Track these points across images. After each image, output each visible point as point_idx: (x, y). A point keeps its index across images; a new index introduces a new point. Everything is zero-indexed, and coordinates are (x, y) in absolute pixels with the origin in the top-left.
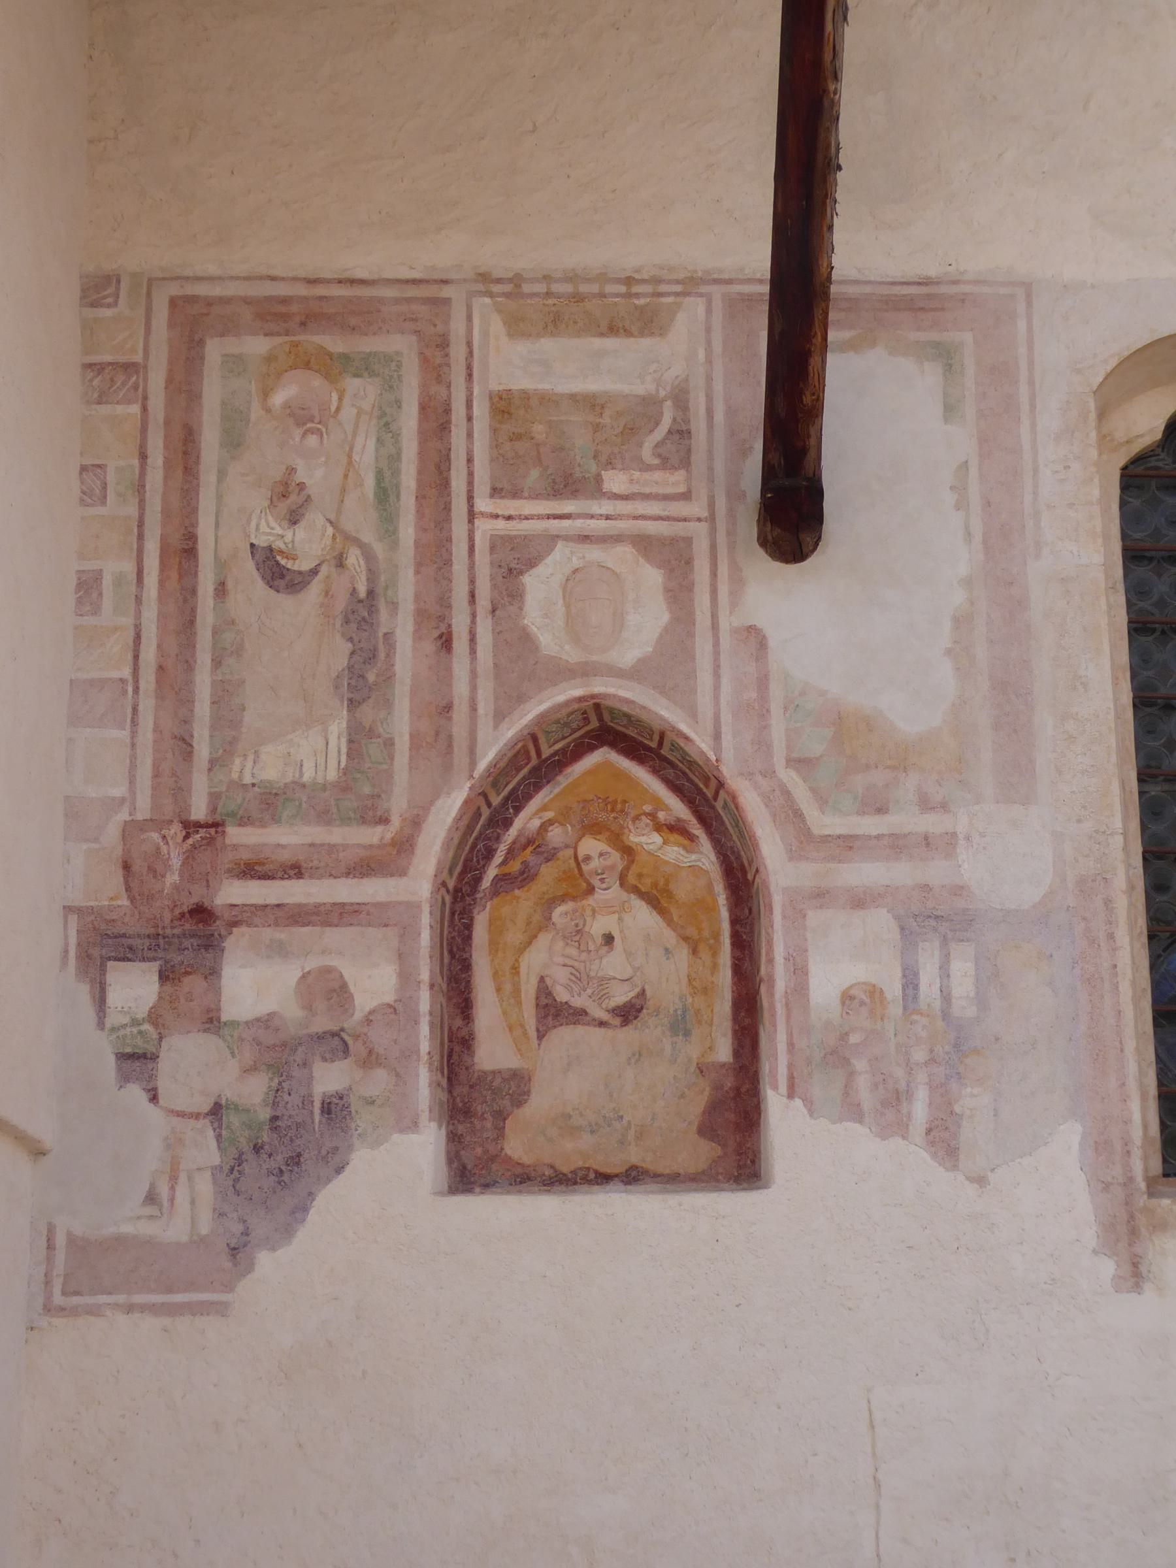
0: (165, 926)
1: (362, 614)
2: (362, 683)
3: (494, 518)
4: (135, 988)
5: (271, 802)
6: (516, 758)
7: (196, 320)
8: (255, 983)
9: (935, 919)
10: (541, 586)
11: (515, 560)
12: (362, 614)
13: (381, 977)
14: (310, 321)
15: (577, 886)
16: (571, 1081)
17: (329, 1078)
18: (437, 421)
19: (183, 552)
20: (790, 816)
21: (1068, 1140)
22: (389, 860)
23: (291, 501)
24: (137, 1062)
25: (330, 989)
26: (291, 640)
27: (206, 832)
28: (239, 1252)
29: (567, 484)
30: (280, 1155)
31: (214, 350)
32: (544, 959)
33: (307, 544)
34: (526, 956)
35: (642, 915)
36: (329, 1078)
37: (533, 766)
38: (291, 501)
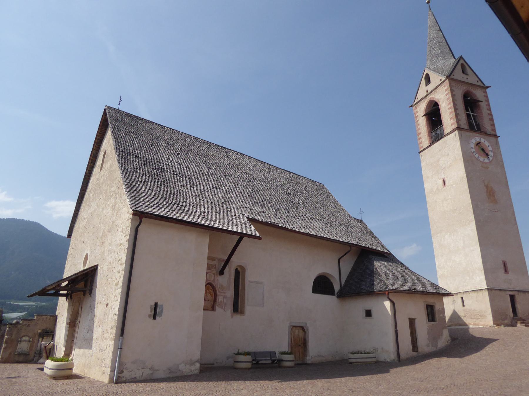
9: (225, 297)
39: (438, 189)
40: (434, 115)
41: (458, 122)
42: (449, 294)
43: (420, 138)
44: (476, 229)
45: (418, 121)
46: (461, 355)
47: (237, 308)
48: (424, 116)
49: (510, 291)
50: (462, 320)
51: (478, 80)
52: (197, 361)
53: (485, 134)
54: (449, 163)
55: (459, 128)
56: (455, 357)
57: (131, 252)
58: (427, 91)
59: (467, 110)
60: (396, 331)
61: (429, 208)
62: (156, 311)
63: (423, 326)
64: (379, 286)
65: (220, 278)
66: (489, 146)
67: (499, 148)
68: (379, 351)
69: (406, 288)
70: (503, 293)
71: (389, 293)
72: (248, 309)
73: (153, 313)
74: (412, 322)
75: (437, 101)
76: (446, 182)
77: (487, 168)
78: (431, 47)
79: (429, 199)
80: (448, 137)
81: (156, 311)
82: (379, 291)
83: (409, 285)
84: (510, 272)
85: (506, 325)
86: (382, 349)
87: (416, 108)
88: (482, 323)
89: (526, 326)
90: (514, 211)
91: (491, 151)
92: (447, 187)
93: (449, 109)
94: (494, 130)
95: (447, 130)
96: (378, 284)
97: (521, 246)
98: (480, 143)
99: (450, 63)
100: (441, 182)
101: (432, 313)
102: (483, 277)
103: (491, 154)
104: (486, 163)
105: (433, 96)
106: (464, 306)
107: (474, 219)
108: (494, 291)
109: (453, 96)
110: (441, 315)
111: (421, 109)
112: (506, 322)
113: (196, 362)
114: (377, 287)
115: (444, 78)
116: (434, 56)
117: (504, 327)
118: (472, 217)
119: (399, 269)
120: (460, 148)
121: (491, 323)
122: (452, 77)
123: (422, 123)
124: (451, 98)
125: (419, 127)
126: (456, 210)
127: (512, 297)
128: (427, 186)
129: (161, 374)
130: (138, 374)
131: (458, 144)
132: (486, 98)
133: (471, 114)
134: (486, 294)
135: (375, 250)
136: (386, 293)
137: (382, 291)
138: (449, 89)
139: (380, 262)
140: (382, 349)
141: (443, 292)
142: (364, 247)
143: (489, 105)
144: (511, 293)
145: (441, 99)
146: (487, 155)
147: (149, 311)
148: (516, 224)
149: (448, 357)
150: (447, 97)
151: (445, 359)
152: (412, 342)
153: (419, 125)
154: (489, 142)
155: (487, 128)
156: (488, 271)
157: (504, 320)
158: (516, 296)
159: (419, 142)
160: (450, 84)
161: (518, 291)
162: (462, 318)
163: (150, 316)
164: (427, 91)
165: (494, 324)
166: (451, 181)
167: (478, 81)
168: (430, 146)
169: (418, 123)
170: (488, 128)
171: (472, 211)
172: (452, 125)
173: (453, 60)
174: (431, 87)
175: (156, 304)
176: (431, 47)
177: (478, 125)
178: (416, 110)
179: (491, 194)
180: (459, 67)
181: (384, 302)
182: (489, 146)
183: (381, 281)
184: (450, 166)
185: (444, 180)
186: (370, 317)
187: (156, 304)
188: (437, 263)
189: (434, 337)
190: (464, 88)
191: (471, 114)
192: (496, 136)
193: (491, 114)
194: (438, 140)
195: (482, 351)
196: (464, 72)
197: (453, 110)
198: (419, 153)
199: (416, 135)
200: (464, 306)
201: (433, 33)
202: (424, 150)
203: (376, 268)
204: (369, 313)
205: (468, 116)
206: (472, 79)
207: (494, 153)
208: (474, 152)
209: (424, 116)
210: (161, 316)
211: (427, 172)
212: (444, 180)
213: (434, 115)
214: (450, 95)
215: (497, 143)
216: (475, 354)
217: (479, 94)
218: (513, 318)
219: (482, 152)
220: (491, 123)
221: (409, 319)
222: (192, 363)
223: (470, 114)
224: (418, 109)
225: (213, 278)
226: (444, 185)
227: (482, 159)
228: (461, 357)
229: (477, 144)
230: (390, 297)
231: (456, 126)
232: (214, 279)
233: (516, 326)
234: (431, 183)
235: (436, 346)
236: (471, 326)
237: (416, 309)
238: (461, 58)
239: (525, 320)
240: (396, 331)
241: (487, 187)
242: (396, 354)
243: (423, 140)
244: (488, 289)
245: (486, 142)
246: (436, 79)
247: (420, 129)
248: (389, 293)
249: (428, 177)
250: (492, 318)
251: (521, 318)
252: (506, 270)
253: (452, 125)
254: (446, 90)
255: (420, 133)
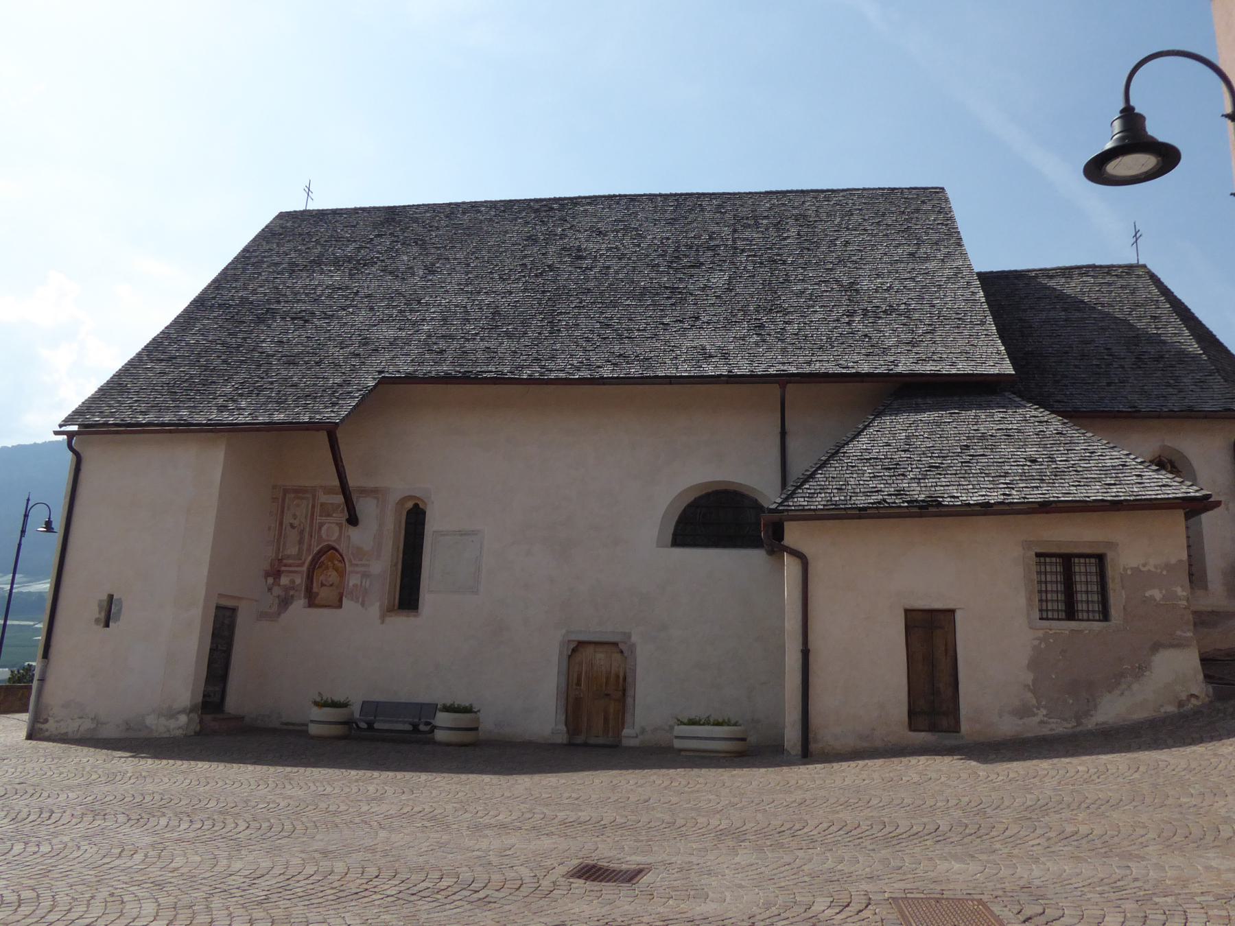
0: (275, 573)
1: (302, 532)
2: (301, 542)
3: (318, 520)
4: (270, 580)
5: (289, 557)
6: (319, 552)
7: (286, 491)
8: (284, 580)
9: (365, 575)
10: (324, 529)
11: (321, 525)
12: (302, 532)
13: (299, 580)
14: (299, 491)
15: (327, 568)
16: (324, 594)
17: (292, 593)
18: (313, 507)
19: (281, 524)
20: (350, 561)
21: (378, 604)
22: (301, 565)
23: (295, 517)
24: (270, 590)
25: (293, 582)
26: (293, 535)
27: (280, 561)
28: (279, 614)
29: (329, 515)
30: (285, 602)
31: (288, 496)
32: (322, 578)
33: (296, 523)
34: (319, 577)
35: (334, 573)
36: (292, 593)
37: (322, 552)
38: (295, 517)
47: (407, 597)
52: (183, 711)
57: (68, 500)
62: (109, 613)
65: (354, 533)
72: (428, 598)
73: (103, 614)
81: (109, 613)
113: (179, 712)
129: (108, 732)
130: (71, 727)
147: (94, 612)
163: (97, 621)
175: (111, 597)
187: (111, 597)
210: (117, 619)
221: (907, 611)
222: (172, 715)
225: (336, 534)
232: (340, 536)
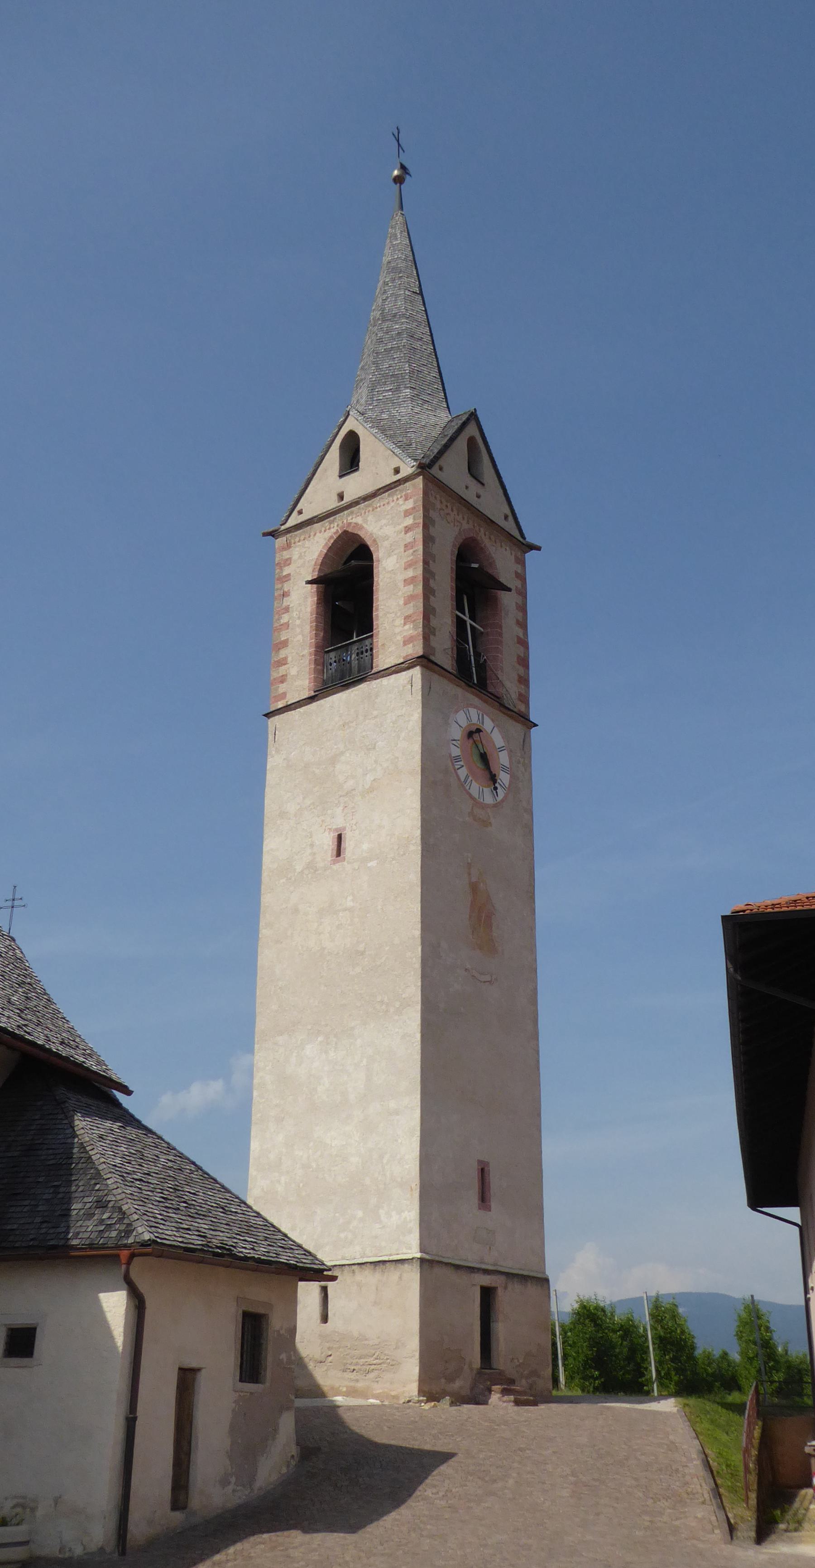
39: (311, 866)
40: (347, 589)
41: (426, 638)
42: (318, 1273)
43: (283, 662)
44: (418, 1036)
45: (285, 595)
46: (351, 1521)
48: (309, 582)
49: (486, 1272)
50: (310, 1376)
51: (508, 511)
53: (498, 702)
54: (369, 778)
55: (425, 661)
56: (331, 1527)
58: (341, 497)
59: (460, 607)
60: (131, 1423)
61: (265, 932)
63: (220, 1397)
64: (90, 1225)
66: (501, 749)
67: (528, 766)
68: (39, 1513)
69: (197, 1242)
70: (462, 1279)
71: (133, 1256)
74: (187, 1378)
75: (369, 543)
76: (348, 844)
77: (486, 823)
78: (380, 341)
79: (272, 897)
80: (385, 681)
82: (91, 1246)
83: (203, 1225)
84: (493, 1205)
85: (459, 1400)
86: (57, 1501)
87: (288, 546)
88: (378, 1389)
89: (517, 1403)
90: (535, 990)
91: (504, 769)
92: (346, 866)
93: (407, 582)
94: (524, 698)
95: (384, 658)
96: (89, 1216)
97: (539, 1115)
98: (479, 731)
99: (433, 420)
100: (328, 842)
101: (258, 1343)
102: (411, 1214)
103: (504, 778)
104: (484, 806)
105: (359, 520)
106: (325, 1318)
107: (418, 998)
108: (438, 1271)
109: (428, 540)
110: (283, 1356)
111: (307, 555)
112: (457, 1385)
114: (84, 1229)
115: (408, 468)
116: (386, 376)
117: (452, 1404)
118: (412, 989)
119: (163, 1159)
120: (418, 730)
121: (412, 1389)
122: (435, 471)
123: (300, 606)
124: (420, 547)
125: (285, 618)
126: (362, 953)
127: (487, 1295)
128: (276, 846)
131: (415, 716)
132: (518, 583)
133: (469, 622)
134: (412, 1278)
135: (80, 1065)
136: (111, 1258)
137: (103, 1247)
138: (420, 513)
139: (98, 1121)
140: (57, 1501)
141: (307, 1262)
142: (41, 1047)
143: (523, 608)
144: (487, 1280)
145: (386, 538)
146: (493, 779)
148: (535, 1036)
149: (305, 1531)
150: (409, 538)
151: (296, 1537)
152: (174, 1465)
153: (287, 609)
154: (506, 737)
155: (508, 684)
156: (432, 1194)
157: (451, 1379)
158: (500, 1292)
159: (275, 675)
160: (426, 493)
161: (507, 1274)
162: (311, 1366)
164: (341, 497)
165: (421, 1392)
166: (365, 846)
167: (506, 517)
168: (311, 699)
169: (286, 602)
170: (509, 688)
171: (418, 965)
172: (405, 643)
173: (444, 417)
174: (356, 485)
176: (380, 341)
177: (482, 667)
178: (286, 554)
179: (482, 915)
180: (461, 444)
181: (102, 1296)
182: (501, 749)
183: (101, 1204)
184: (371, 790)
185: (340, 837)
186: (25, 1361)
188: (255, 1146)
189: (247, 1447)
190: (466, 526)
191: (469, 622)
192: (528, 724)
193: (523, 643)
194: (347, 686)
195: (411, 1502)
196: (473, 469)
197: (420, 588)
198: (268, 715)
199: (273, 646)
200: (325, 1318)
201: (397, 296)
202: (288, 708)
203: (82, 1146)
204: (22, 1343)
205: (460, 624)
206: (490, 504)
207: (514, 778)
208: (457, 759)
209: (309, 582)
211: (281, 791)
212: (340, 837)
213: (347, 589)
214: (418, 534)
215: (525, 743)
216: (394, 1515)
217: (501, 561)
218: (479, 1373)
219: (479, 765)
220: (521, 670)
221: (180, 1369)
223: (465, 622)
224: (295, 553)
226: (339, 853)
227: (475, 788)
228: (353, 1528)
229: (470, 734)
230: (133, 1275)
231: (416, 649)
233: (485, 1403)
234: (289, 838)
235: (252, 1478)
236: (339, 1400)
237: (200, 1328)
238: (473, 416)
239: (512, 1382)
240: (131, 1423)
241: (474, 888)
242: (112, 1524)
243: (293, 671)
244: (422, 1260)
245: (496, 735)
246: (380, 461)
247: (287, 625)
248: (133, 1256)
249: (283, 815)
250: (416, 1370)
251: (501, 1373)
252: (484, 1198)
253: (405, 643)
254: (407, 513)
255: (285, 644)
